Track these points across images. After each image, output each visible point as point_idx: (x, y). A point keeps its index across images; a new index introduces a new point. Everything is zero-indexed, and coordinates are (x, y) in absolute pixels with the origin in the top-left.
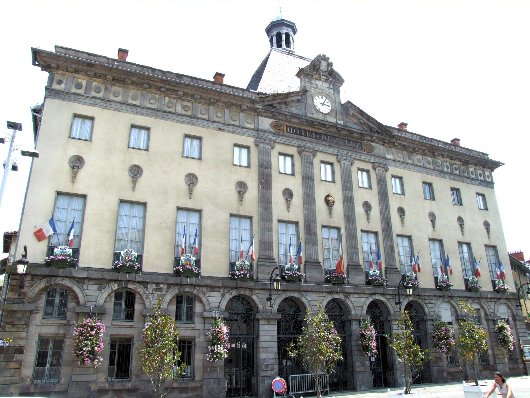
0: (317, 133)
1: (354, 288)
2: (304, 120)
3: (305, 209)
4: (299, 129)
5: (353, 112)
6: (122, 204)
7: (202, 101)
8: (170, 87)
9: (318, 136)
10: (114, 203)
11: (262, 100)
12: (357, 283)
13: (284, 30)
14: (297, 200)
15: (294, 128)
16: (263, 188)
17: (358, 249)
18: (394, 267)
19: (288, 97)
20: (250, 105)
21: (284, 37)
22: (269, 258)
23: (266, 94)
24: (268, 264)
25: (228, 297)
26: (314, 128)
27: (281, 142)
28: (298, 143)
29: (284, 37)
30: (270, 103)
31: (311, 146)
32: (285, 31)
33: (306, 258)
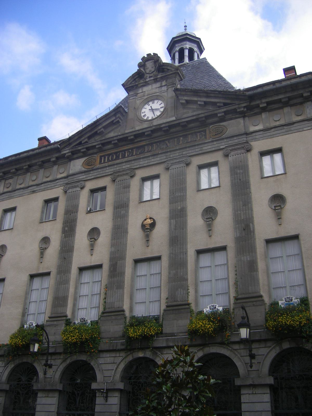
0: (138, 148)
1: (167, 340)
2: (116, 141)
3: (112, 245)
4: (116, 153)
5: (186, 98)
6: (270, 245)
7: (19, 172)
8: (231, 142)
9: (140, 151)
10: (25, 278)
11: (68, 143)
12: (175, 331)
13: (188, 45)
14: (104, 239)
15: (109, 155)
16: (65, 237)
17: (187, 280)
18: (258, 294)
19: (97, 126)
20: (57, 155)
21: (186, 53)
22: (62, 315)
23: (291, 106)
24: (55, 323)
25: (11, 366)
26: (133, 143)
27: (93, 177)
28: (112, 170)
29: (186, 53)
30: (78, 142)
31: (129, 166)
32: (188, 46)
33: (237, 291)
